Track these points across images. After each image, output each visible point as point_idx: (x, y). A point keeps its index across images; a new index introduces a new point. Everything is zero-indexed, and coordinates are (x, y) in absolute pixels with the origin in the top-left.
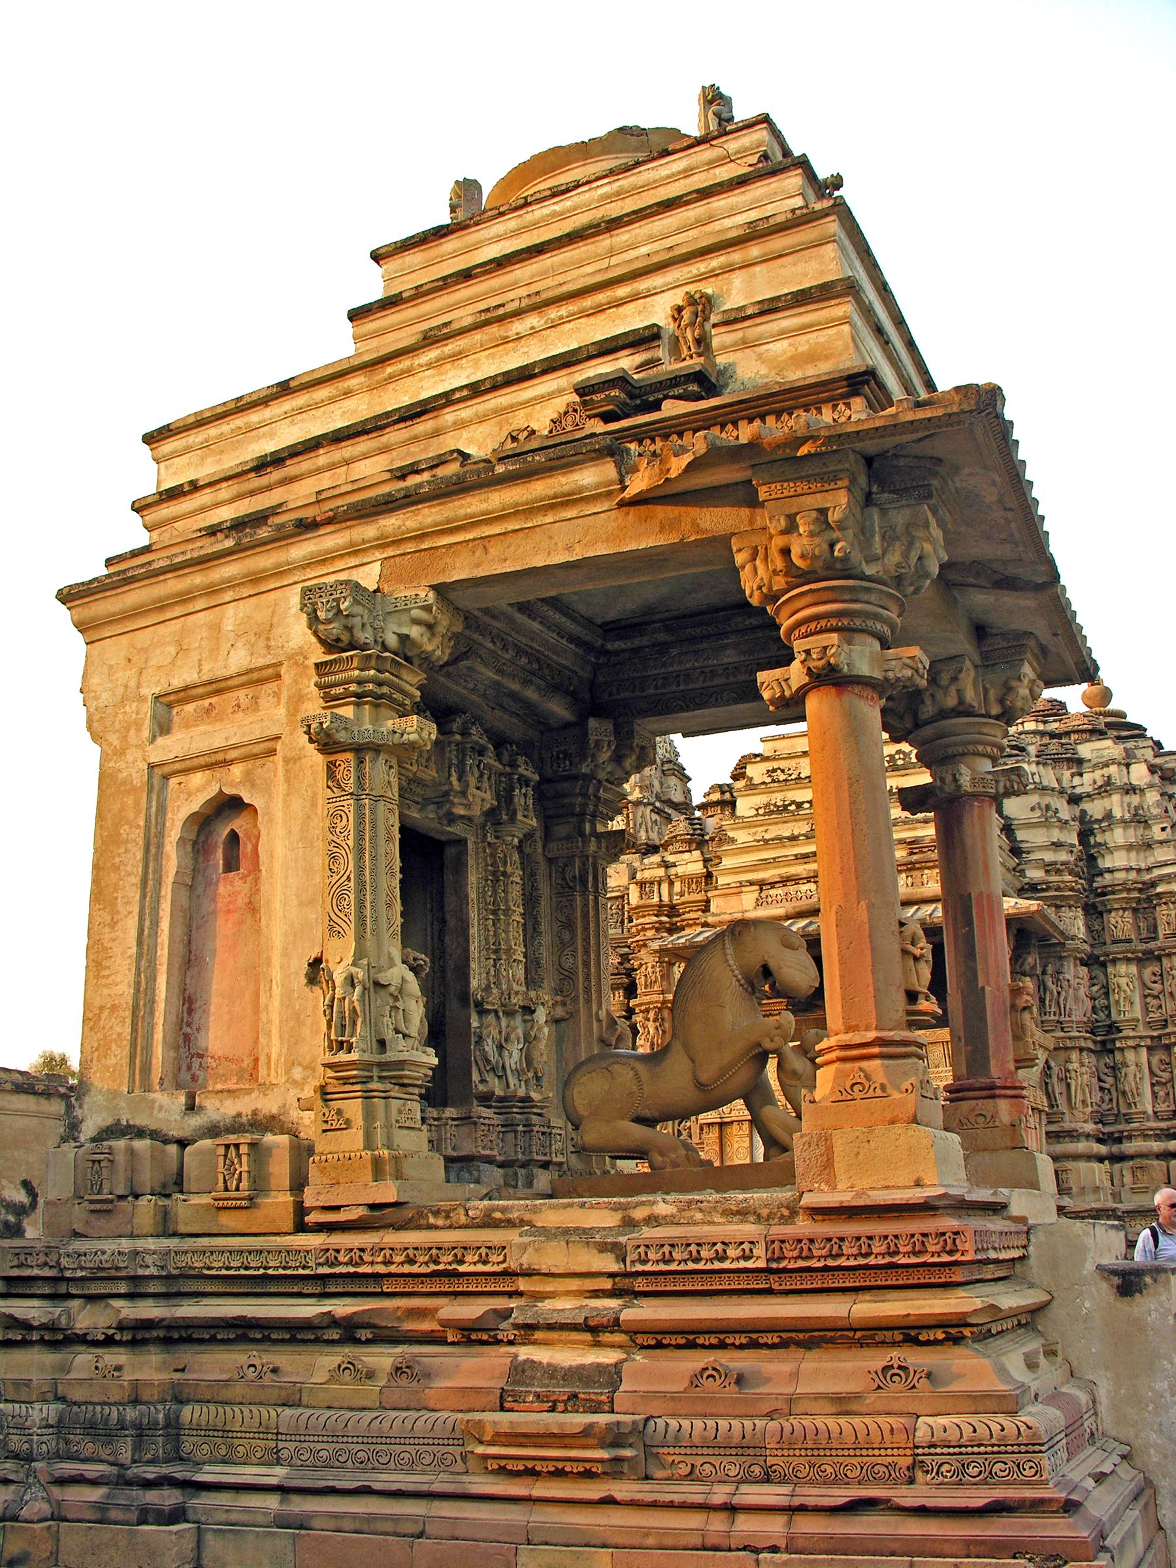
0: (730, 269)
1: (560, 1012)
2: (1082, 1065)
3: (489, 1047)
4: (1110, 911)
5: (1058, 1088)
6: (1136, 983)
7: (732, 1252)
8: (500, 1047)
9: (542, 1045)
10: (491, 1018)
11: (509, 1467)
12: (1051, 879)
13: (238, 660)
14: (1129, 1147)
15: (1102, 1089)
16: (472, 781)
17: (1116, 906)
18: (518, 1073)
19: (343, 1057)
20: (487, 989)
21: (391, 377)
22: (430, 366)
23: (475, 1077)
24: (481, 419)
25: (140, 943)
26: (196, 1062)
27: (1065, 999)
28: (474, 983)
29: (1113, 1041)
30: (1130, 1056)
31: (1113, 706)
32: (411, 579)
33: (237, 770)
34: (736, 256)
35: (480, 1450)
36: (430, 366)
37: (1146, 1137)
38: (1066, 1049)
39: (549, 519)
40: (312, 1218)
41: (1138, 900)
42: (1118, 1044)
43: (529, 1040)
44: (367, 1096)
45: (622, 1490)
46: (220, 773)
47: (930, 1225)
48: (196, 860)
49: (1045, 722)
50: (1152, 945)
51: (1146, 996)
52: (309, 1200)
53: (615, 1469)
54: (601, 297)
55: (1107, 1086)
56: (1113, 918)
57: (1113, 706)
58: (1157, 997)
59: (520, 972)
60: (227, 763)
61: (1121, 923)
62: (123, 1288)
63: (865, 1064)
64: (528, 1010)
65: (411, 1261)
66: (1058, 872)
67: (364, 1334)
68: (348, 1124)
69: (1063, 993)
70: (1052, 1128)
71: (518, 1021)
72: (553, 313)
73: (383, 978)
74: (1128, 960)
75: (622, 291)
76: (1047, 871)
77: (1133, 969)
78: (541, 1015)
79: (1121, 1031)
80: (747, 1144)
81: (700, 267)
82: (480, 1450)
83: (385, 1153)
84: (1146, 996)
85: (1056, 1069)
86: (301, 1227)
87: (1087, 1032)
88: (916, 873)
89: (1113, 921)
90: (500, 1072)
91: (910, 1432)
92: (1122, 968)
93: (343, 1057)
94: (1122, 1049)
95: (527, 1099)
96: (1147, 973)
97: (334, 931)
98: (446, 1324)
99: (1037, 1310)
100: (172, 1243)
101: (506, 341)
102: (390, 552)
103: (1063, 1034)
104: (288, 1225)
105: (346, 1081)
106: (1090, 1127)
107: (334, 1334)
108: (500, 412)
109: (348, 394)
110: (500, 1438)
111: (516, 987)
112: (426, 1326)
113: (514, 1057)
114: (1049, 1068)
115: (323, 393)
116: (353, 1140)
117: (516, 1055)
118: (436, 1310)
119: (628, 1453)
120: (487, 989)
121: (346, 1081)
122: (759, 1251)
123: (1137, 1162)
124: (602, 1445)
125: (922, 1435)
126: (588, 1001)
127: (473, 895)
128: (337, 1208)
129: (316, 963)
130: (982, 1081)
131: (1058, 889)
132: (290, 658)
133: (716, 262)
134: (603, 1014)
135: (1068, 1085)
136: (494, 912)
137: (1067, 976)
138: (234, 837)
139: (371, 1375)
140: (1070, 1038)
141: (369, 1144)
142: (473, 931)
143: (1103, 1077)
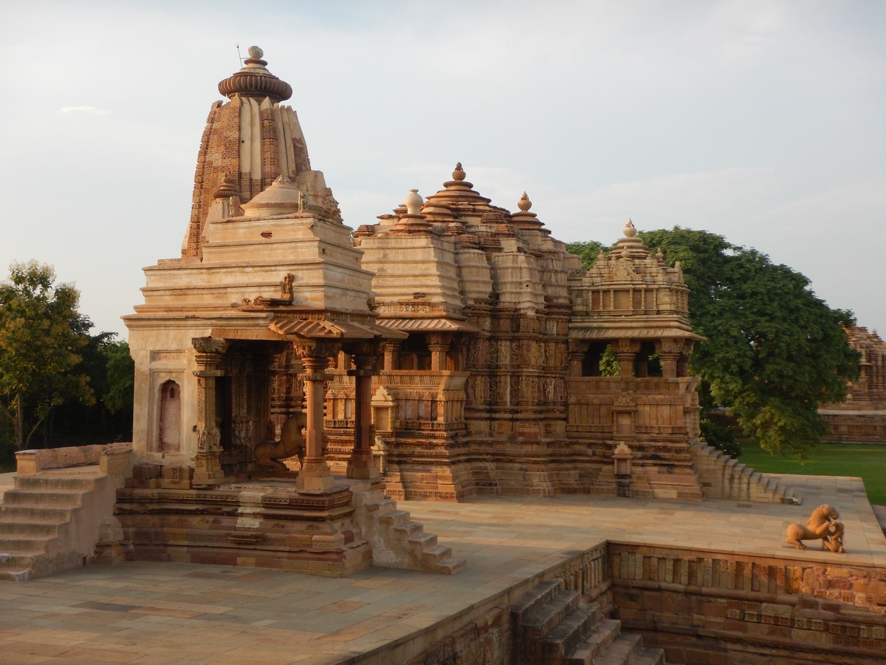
0: (298, 270)
1: (256, 420)
2: (482, 382)
3: (237, 433)
4: (501, 318)
5: (470, 391)
6: (508, 349)
7: (283, 501)
8: (239, 432)
9: (251, 431)
10: (237, 425)
11: (428, 309)
12: (476, 305)
13: (174, 347)
14: (497, 415)
15: (491, 390)
16: (233, 367)
17: (504, 317)
18: (244, 438)
19: (202, 451)
20: (236, 417)
21: (214, 272)
22: (224, 273)
23: (233, 440)
24: (237, 293)
25: (148, 415)
26: (164, 445)
27: (477, 355)
28: (233, 415)
29: (497, 372)
30: (503, 379)
31: (530, 211)
32: (220, 336)
33: (174, 374)
34: (300, 267)
35: (230, 538)
36: (224, 273)
37: (506, 412)
38: (475, 375)
39: (252, 328)
40: (194, 487)
41: (513, 315)
42: (498, 374)
43: (247, 430)
44: (207, 459)
45: (258, 547)
46: (170, 374)
47: (320, 499)
48: (163, 394)
49: (490, 227)
50: (516, 334)
51: (512, 355)
52: (193, 483)
53: (256, 543)
54: (268, 268)
55: (493, 389)
56: (502, 322)
57: (530, 211)
58: (516, 355)
59: (245, 411)
60: (171, 372)
61: (505, 324)
62: (148, 501)
63: (312, 464)
64: (247, 422)
65: (217, 498)
66: (480, 303)
67: (206, 513)
68: (203, 466)
69: (476, 353)
70: (468, 406)
71: (245, 425)
72: (256, 269)
73: (211, 432)
74: (506, 340)
75: (273, 268)
76: (475, 302)
77: (508, 343)
78: (251, 423)
79: (500, 368)
80: (343, 408)
81: (292, 267)
82: (230, 538)
83: (211, 473)
84: (512, 355)
85: (470, 384)
86: (191, 488)
87: (486, 368)
88: (416, 307)
89: (502, 323)
90: (239, 438)
91: (311, 538)
92: (504, 343)
93: (202, 451)
94: (500, 376)
95: (246, 445)
96: (514, 345)
97: (199, 419)
98: (224, 512)
99: (352, 512)
100: (160, 490)
101: (243, 272)
102: (214, 328)
103: (475, 370)
104: (188, 487)
105: (203, 456)
106: (481, 407)
107: (199, 513)
108: (242, 292)
109: (202, 273)
110: (235, 536)
111: (244, 415)
112: (219, 512)
113: (243, 434)
114: (468, 382)
115: (195, 271)
116: (204, 469)
117: (244, 434)
118: (222, 509)
119: (259, 540)
120: (236, 417)
121: (203, 456)
122: (288, 501)
123: (501, 422)
124: (254, 538)
125: (313, 539)
126: (264, 417)
127: (233, 391)
128: (200, 485)
129: (195, 427)
130: (360, 450)
131: (479, 310)
132: (188, 349)
133: (295, 267)
134: (268, 420)
135: (475, 390)
136: (239, 395)
137: (479, 346)
138: (172, 389)
139: (208, 522)
140: (477, 371)
141: (207, 471)
142: (233, 401)
143: (493, 386)
